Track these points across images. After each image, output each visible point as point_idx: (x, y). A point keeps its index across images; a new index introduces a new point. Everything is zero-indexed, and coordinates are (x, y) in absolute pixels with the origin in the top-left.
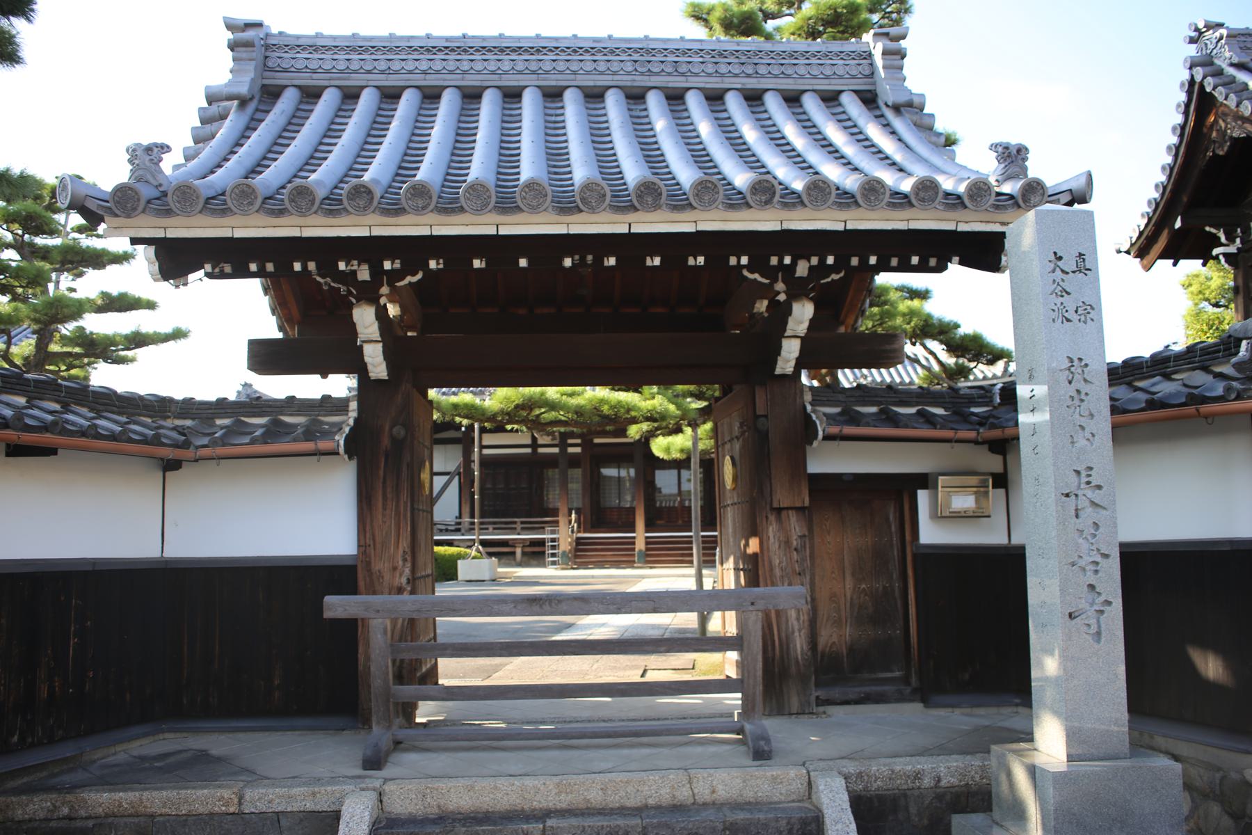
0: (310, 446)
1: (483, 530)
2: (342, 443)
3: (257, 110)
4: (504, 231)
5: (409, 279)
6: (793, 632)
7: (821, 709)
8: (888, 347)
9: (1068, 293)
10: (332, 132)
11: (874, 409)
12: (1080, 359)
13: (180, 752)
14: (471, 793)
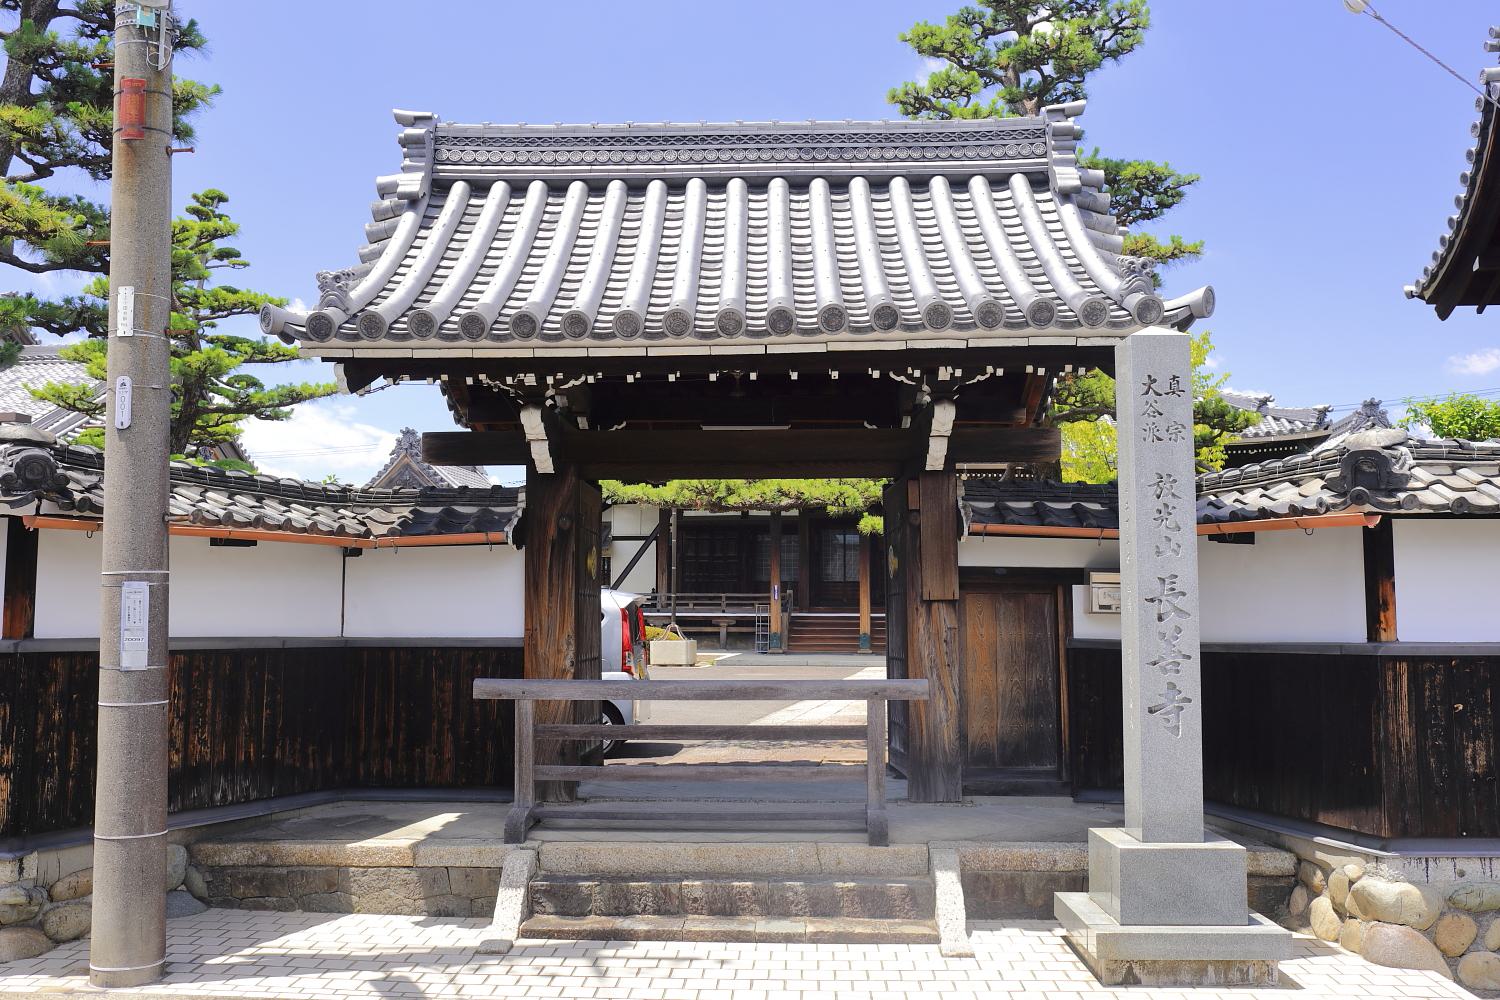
0: (481, 537)
1: (681, 603)
2: (510, 535)
3: (429, 205)
4: (653, 353)
5: (572, 383)
6: (941, 722)
7: (969, 798)
8: (1043, 442)
9: (1161, 414)
10: (497, 233)
11: (1028, 505)
12: (1170, 476)
13: (359, 817)
14: (619, 855)
